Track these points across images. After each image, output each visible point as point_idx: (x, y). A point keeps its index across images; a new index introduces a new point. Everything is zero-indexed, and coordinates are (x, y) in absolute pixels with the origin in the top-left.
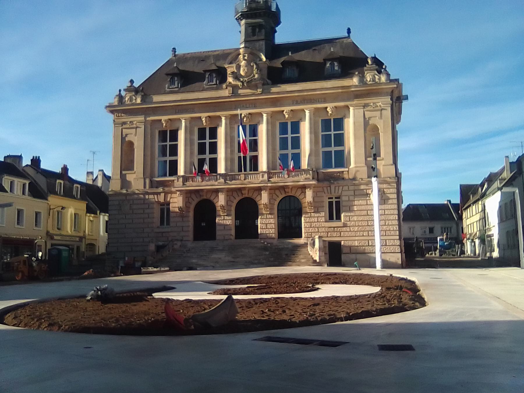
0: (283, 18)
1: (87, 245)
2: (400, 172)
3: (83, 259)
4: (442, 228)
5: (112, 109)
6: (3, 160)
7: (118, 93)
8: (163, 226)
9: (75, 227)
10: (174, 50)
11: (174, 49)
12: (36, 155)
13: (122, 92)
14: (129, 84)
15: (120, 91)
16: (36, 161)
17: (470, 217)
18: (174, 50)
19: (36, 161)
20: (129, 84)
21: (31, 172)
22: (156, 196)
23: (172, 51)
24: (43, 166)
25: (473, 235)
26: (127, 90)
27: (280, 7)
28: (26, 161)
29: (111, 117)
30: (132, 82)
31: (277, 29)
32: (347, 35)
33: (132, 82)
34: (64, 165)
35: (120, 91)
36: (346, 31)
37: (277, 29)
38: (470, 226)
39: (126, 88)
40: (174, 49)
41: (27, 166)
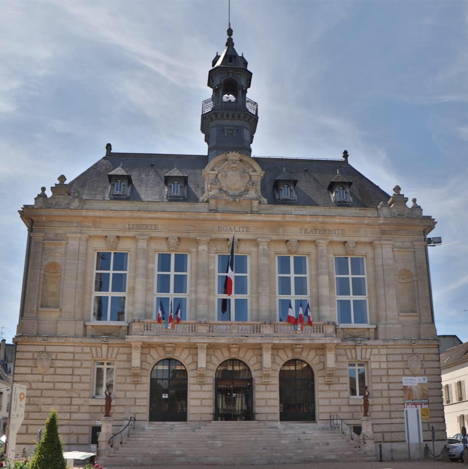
15: (43, 189)
32: (343, 159)
35: (43, 189)
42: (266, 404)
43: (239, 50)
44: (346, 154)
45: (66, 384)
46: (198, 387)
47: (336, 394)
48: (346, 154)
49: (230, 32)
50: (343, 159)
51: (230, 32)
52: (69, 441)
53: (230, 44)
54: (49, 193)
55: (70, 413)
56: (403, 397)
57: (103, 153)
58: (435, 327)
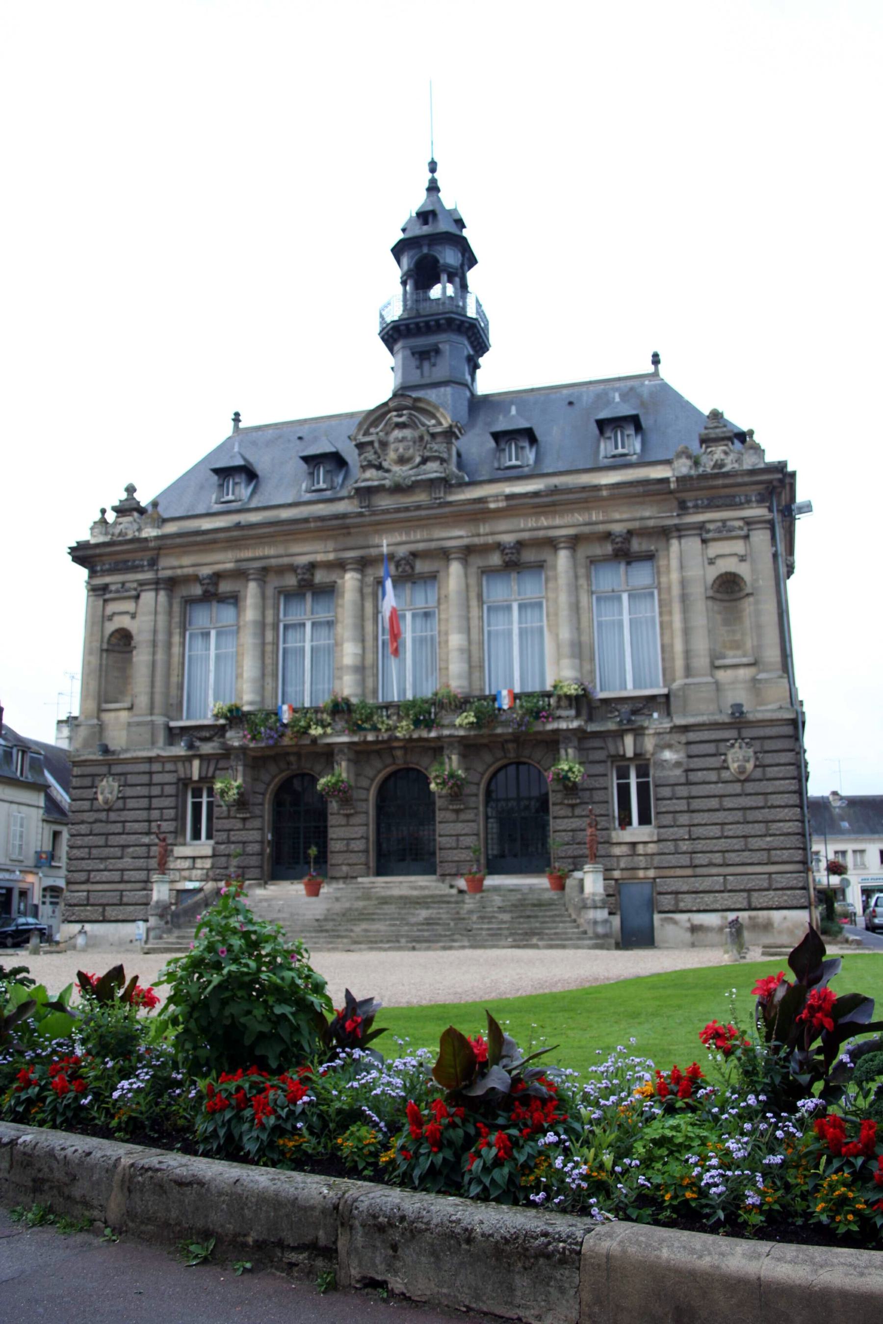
1: (45, 889)
2: (800, 698)
3: (734, 990)
5: (82, 554)
7: (98, 516)
10: (237, 418)
11: (237, 414)
13: (107, 516)
15: (103, 511)
18: (237, 418)
20: (124, 496)
22: (180, 765)
26: (120, 511)
27: (481, 302)
29: (83, 573)
30: (131, 490)
31: (481, 361)
32: (651, 369)
33: (131, 490)
35: (103, 511)
36: (427, 168)
37: (481, 361)
40: (237, 414)
41: (70, 738)
42: (725, 880)
43: (448, 199)
44: (656, 360)
45: (708, 758)
46: (450, 816)
47: (238, 849)
48: (656, 360)
49: (433, 167)
50: (651, 369)
51: (433, 167)
52: (840, 915)
53: (433, 188)
54: (111, 517)
55: (149, 821)
56: (660, 893)
57: (228, 430)
58: (801, 747)
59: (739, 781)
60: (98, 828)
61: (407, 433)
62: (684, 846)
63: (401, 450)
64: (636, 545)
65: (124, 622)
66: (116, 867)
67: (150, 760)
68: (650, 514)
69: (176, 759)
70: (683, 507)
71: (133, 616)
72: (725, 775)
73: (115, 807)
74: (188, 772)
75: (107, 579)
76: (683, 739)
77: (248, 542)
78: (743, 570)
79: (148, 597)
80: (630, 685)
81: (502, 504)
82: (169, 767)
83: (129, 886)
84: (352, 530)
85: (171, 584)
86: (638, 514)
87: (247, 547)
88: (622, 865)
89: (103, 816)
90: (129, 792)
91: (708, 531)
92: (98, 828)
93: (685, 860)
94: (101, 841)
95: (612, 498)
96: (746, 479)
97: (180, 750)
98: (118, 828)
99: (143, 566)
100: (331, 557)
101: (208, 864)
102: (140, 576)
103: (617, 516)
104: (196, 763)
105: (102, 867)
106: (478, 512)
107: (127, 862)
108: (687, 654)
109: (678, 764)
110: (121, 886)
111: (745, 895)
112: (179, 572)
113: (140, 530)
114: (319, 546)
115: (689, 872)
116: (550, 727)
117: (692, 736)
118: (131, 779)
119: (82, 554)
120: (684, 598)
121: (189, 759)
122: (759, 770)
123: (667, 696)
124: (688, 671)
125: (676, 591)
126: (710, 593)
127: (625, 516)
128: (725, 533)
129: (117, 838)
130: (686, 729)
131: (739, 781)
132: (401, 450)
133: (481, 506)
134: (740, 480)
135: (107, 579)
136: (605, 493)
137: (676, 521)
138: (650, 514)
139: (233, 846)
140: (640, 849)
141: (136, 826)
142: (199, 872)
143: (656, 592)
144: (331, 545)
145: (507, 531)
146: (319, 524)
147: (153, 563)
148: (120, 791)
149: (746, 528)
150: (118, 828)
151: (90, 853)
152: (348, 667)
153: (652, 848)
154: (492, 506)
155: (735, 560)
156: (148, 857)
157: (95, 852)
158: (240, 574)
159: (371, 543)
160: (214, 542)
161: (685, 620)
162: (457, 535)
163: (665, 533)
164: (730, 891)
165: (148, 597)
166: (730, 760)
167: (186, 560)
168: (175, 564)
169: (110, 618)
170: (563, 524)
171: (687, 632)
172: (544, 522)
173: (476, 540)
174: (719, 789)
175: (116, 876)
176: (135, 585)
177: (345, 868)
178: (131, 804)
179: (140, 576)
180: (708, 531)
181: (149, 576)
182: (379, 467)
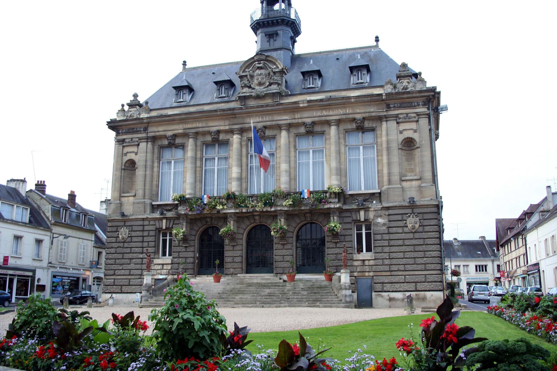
0: (303, 28)
1: (94, 278)
4: (476, 266)
5: (113, 125)
6: (5, 184)
8: (164, 257)
9: (246, 304)
10: (185, 63)
11: (185, 62)
12: (41, 179)
14: (132, 98)
15: (123, 106)
16: (41, 187)
17: (508, 253)
18: (185, 63)
19: (41, 187)
20: (132, 98)
21: (36, 199)
22: (157, 222)
23: (183, 64)
24: (48, 191)
25: (512, 273)
28: (31, 186)
29: (113, 134)
30: (135, 96)
33: (135, 96)
34: (72, 191)
35: (123, 106)
38: (508, 263)
39: (129, 102)
40: (185, 62)
59: (412, 232)
60: (119, 250)
61: (263, 71)
62: (387, 262)
63: (260, 79)
64: (367, 124)
65: (132, 156)
66: (127, 268)
67: (143, 219)
68: (374, 110)
69: (155, 219)
70: (388, 107)
71: (136, 154)
72: (406, 230)
73: (127, 241)
74: (161, 225)
75: (124, 137)
76: (387, 213)
77: (189, 120)
78: (415, 136)
79: (143, 145)
80: (363, 188)
81: (306, 105)
82: (152, 223)
83: (133, 277)
84: (237, 116)
85: (154, 139)
86: (368, 110)
87: (188, 123)
88: (358, 270)
89: (121, 245)
90: (134, 234)
91: (400, 118)
92: (119, 250)
93: (387, 268)
94: (120, 256)
95: (355, 103)
96: (418, 95)
97: (157, 215)
98: (128, 250)
99: (141, 131)
100: (227, 128)
101: (169, 267)
102: (140, 136)
103: (358, 111)
104: (164, 221)
105: (121, 268)
106: (295, 108)
107: (132, 266)
108: (389, 174)
109: (384, 224)
110: (130, 277)
111: (414, 284)
112: (157, 134)
113: (139, 114)
114: (221, 123)
115: (389, 273)
116: (326, 207)
117: (391, 212)
118: (135, 228)
119: (113, 125)
120: (388, 149)
121: (161, 219)
122: (130, 238)
123: (380, 193)
124: (390, 182)
125: (384, 145)
126: (400, 147)
127: (362, 111)
128: (407, 119)
129: (128, 255)
130: (388, 208)
131: (412, 232)
132: (260, 79)
133: (296, 105)
134: (414, 95)
135: (124, 137)
136: (353, 100)
137: (385, 113)
138: (374, 110)
139: (181, 259)
140: (367, 263)
141: (137, 249)
142: (165, 271)
143: (375, 146)
144: (227, 122)
145: (308, 117)
146: (222, 113)
147: (146, 129)
148: (129, 234)
149: (417, 117)
150: (128, 250)
151: (115, 262)
152: (234, 178)
153: (372, 263)
154: (301, 105)
155: (412, 132)
156: (142, 264)
157: (117, 261)
158: (185, 135)
159: (245, 122)
160: (174, 120)
161: (389, 159)
162: (285, 119)
163: (380, 119)
164: (407, 282)
165: (143, 145)
166: (408, 223)
167: (161, 129)
168: (154, 130)
169: (401, 132)
170: (334, 114)
171: (389, 164)
172: (325, 113)
173: (294, 121)
174: (403, 236)
175: (127, 272)
176: (137, 139)
177: (232, 270)
178: (134, 239)
179: (140, 136)
180: (400, 118)
181: (144, 135)
182: (250, 87)
